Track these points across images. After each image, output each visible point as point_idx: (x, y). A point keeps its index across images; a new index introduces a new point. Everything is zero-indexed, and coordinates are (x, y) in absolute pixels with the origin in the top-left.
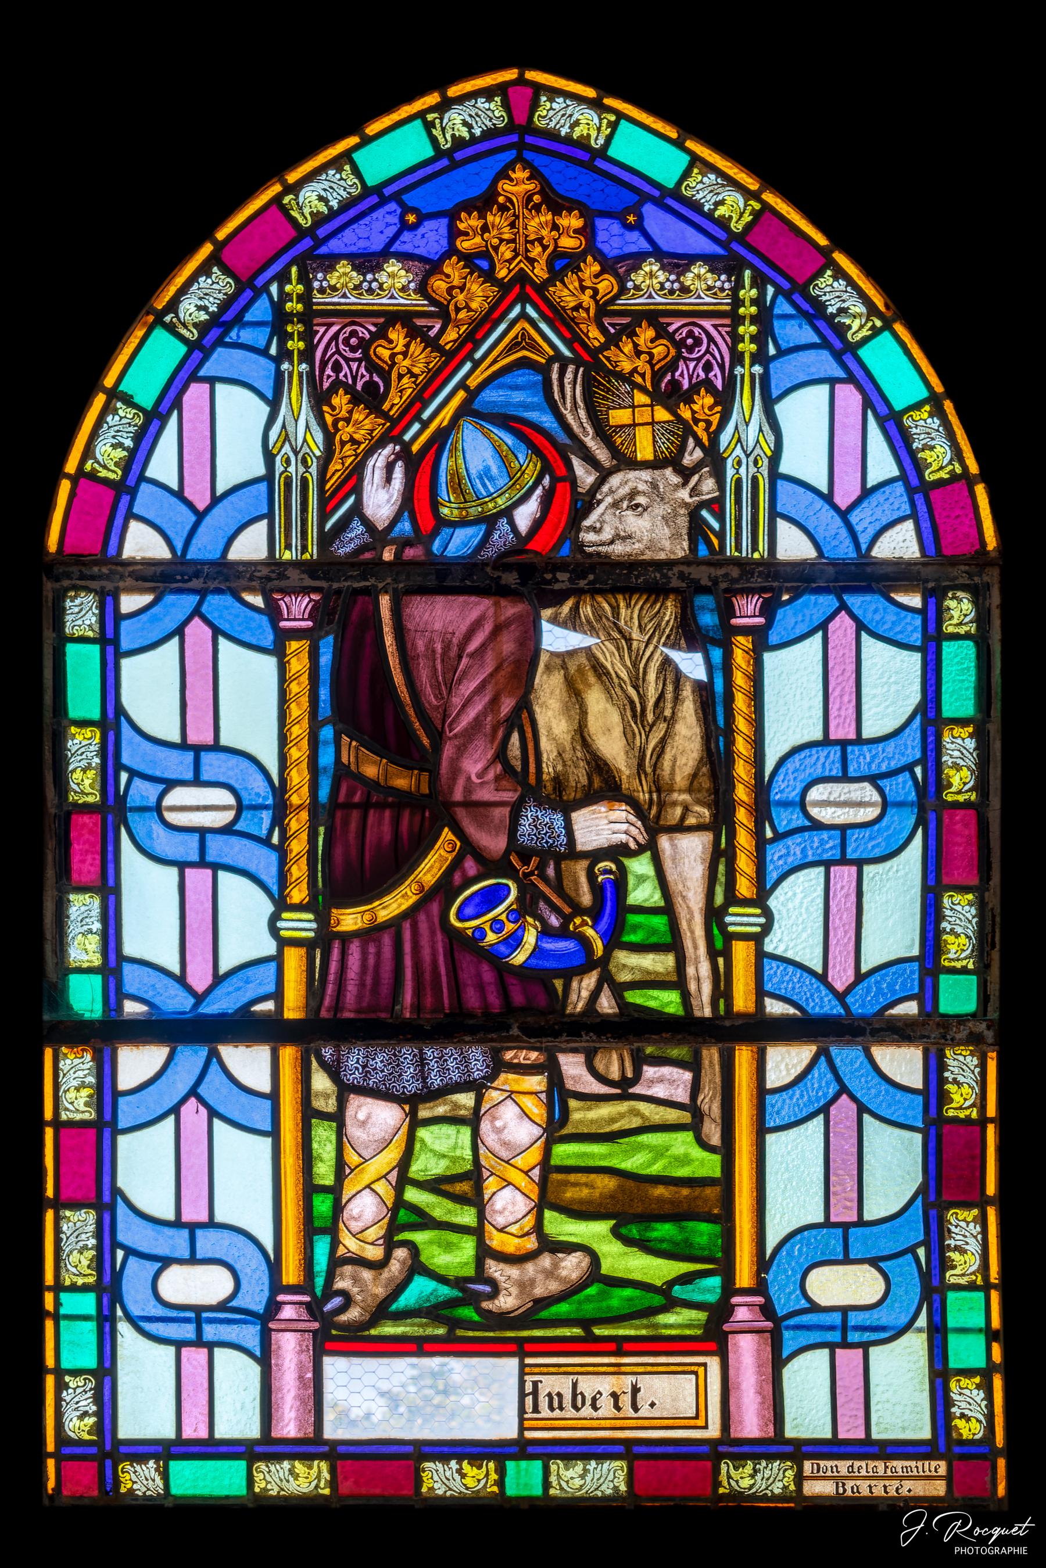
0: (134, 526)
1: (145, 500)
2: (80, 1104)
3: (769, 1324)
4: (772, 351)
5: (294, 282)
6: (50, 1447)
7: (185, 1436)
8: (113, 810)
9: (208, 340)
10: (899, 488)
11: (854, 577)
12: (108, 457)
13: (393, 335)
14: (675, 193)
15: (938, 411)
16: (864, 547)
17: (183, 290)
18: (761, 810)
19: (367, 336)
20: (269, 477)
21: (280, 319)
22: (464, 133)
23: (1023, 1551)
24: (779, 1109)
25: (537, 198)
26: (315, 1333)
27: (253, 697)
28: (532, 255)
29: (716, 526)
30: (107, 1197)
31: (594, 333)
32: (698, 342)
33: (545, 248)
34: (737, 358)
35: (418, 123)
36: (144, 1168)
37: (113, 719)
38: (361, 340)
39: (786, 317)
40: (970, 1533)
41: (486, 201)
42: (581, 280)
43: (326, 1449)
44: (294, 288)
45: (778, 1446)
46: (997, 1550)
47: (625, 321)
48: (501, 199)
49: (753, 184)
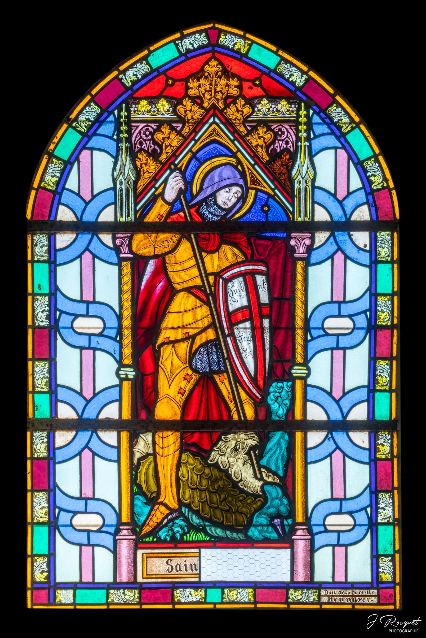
0: (61, 208)
1: (66, 197)
2: (42, 450)
3: (309, 537)
4: (312, 136)
5: (124, 111)
6: (29, 585)
7: (84, 580)
8: (54, 327)
9: (90, 134)
10: (362, 192)
11: (343, 226)
12: (51, 180)
13: (163, 130)
14: (275, 71)
15: (377, 161)
16: (348, 216)
17: (80, 113)
18: (307, 329)
19: (152, 131)
20: (114, 188)
21: (118, 123)
22: (191, 47)
23: (416, 631)
24: (312, 455)
25: (220, 73)
26: (134, 540)
27: (108, 284)
28: (218, 97)
29: (291, 209)
30: (52, 487)
31: (242, 129)
32: (283, 133)
33: (223, 94)
34: (298, 139)
35: (172, 44)
36: (67, 477)
37: (54, 291)
38: (150, 132)
39: (319, 124)
40: (395, 624)
41: (199, 74)
42: (237, 108)
43: (138, 585)
44: (124, 113)
45: (310, 584)
46: (406, 631)
47: (254, 124)
48: (206, 74)
49: (305, 69)
